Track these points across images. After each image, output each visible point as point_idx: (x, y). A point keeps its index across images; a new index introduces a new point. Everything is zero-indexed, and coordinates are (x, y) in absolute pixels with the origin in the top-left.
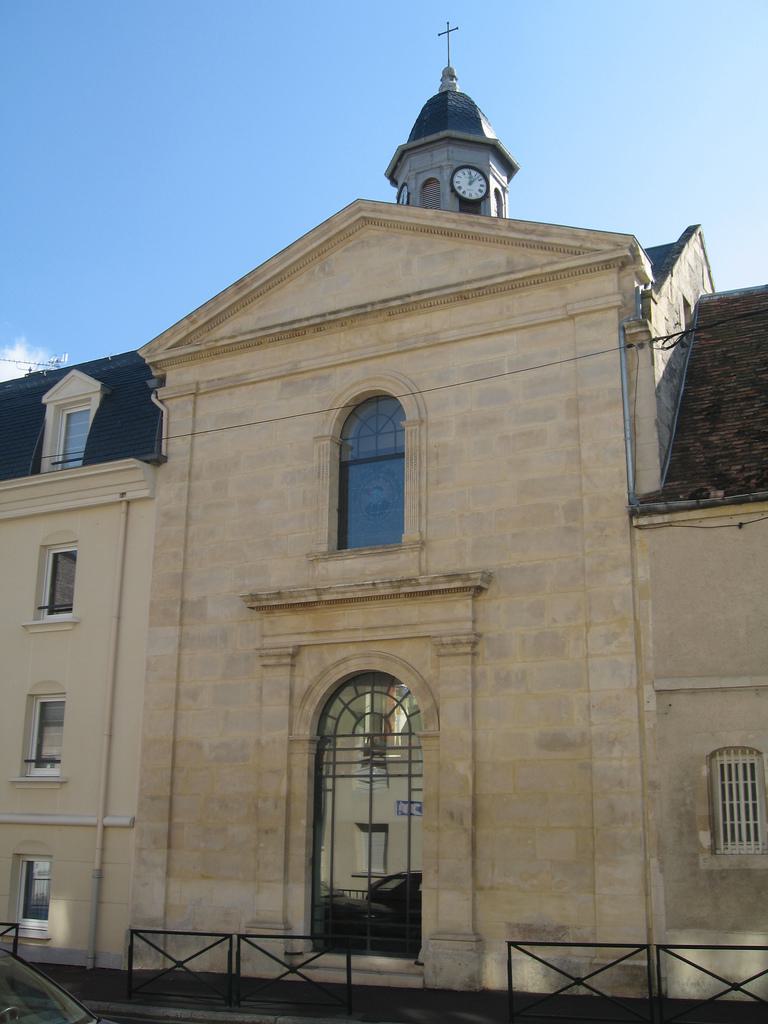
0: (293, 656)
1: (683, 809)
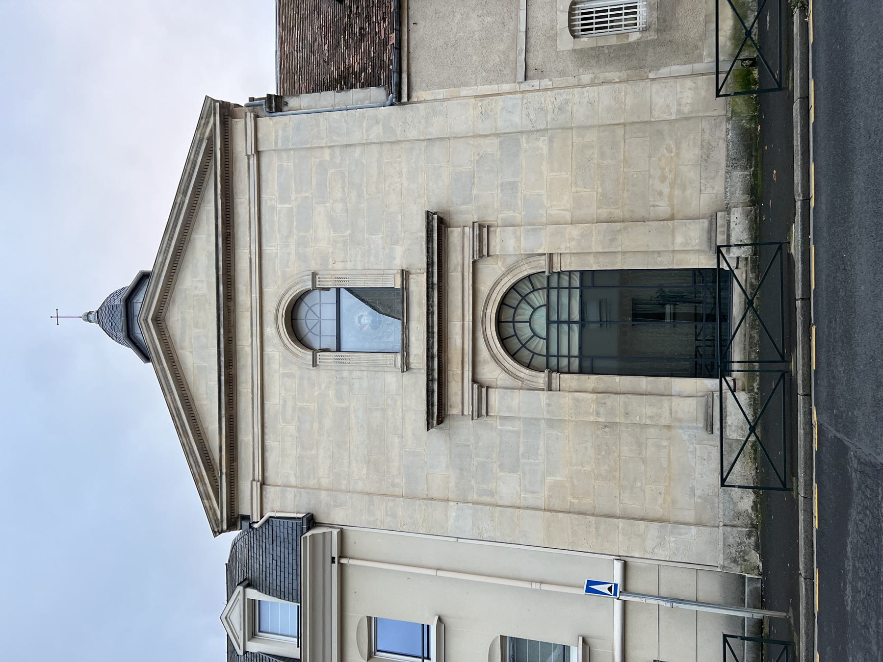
0: (480, 387)
1: (612, 55)
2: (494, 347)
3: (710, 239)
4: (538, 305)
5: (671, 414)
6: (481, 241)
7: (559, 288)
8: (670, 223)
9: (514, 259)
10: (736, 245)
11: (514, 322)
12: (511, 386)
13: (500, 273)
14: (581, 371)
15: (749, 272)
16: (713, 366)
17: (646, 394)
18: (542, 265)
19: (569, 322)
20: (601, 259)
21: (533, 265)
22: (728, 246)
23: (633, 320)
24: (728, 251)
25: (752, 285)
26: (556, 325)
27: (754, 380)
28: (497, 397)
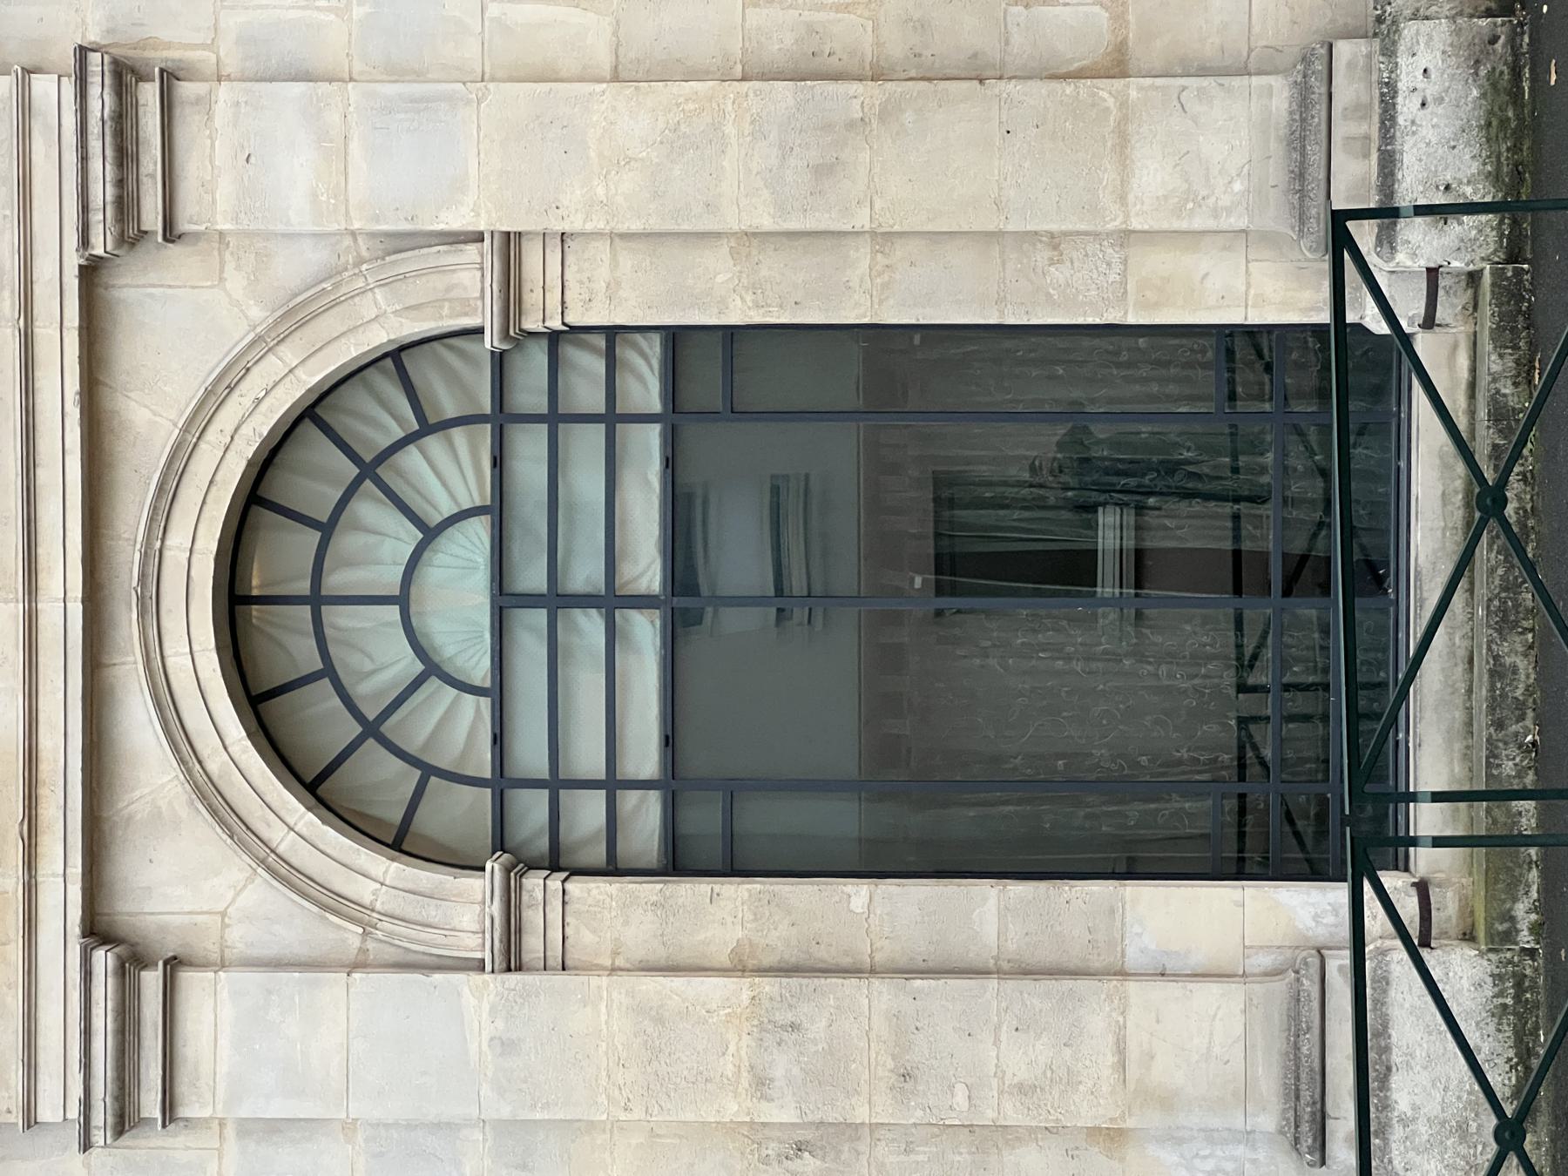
0: (133, 961)
2: (207, 743)
3: (1300, 175)
4: (447, 509)
5: (1122, 1065)
6: (125, 154)
7: (555, 418)
8: (1106, 91)
9: (314, 258)
10: (1421, 210)
11: (317, 600)
12: (303, 952)
13: (237, 335)
14: (677, 862)
15: (1486, 345)
16: (1322, 818)
17: (1000, 973)
18: (462, 293)
19: (612, 601)
20: (771, 265)
21: (419, 291)
22: (1387, 213)
23: (940, 590)
24: (1387, 241)
25: (1499, 414)
26: (540, 617)
27: (1514, 888)
28: (227, 1013)
